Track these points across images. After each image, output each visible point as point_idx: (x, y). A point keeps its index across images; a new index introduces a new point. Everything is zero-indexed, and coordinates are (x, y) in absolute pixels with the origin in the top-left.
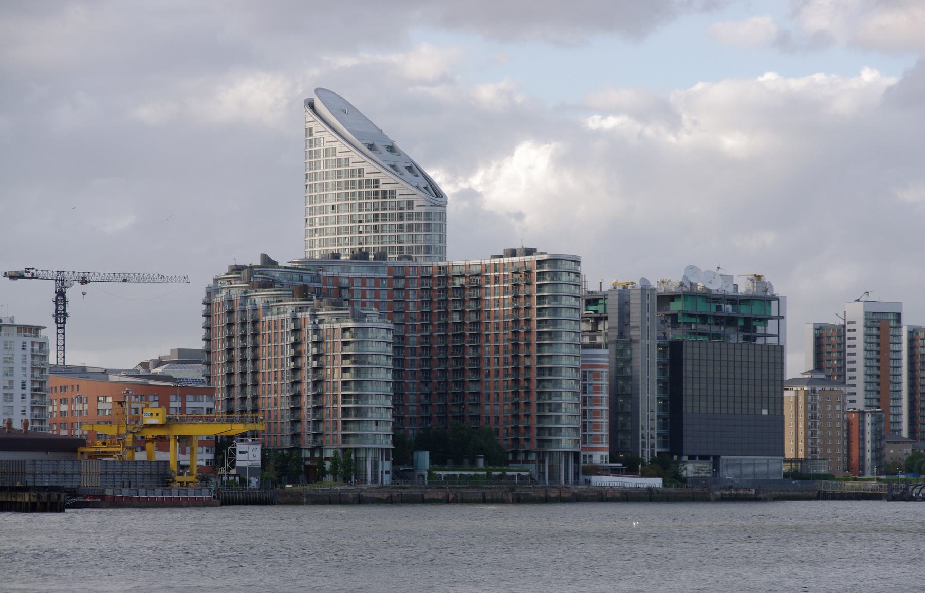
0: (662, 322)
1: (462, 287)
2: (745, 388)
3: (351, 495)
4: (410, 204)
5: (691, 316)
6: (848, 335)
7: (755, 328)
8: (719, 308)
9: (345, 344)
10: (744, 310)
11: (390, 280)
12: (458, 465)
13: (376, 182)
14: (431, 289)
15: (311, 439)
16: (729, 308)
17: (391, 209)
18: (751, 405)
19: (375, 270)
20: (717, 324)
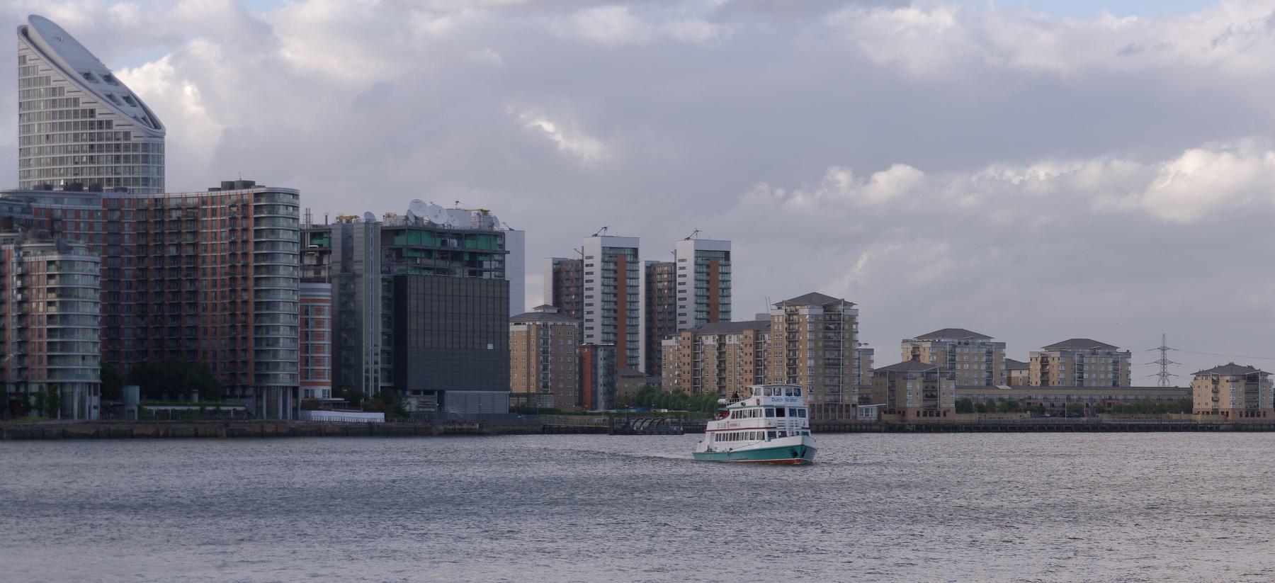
0: (387, 256)
1: (179, 220)
2: (470, 323)
3: (55, 431)
4: (127, 135)
5: (416, 250)
6: (586, 269)
7: (481, 263)
8: (444, 243)
9: (51, 277)
10: (470, 245)
11: (104, 213)
12: (173, 399)
13: (92, 112)
14: (146, 222)
15: (15, 373)
16: (454, 243)
17: (108, 139)
18: (477, 340)
19: (88, 201)
20: (443, 258)
